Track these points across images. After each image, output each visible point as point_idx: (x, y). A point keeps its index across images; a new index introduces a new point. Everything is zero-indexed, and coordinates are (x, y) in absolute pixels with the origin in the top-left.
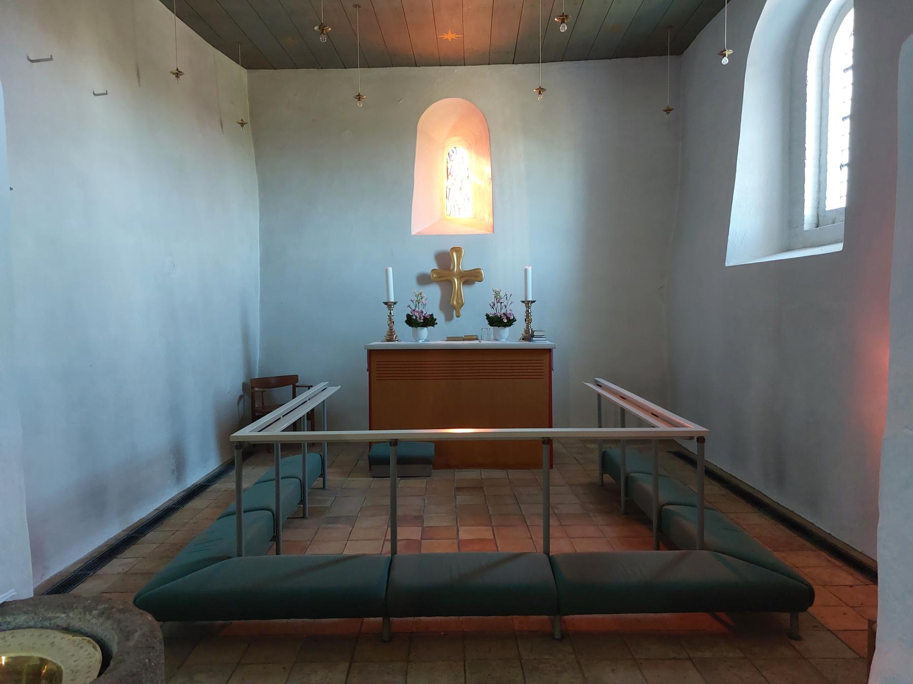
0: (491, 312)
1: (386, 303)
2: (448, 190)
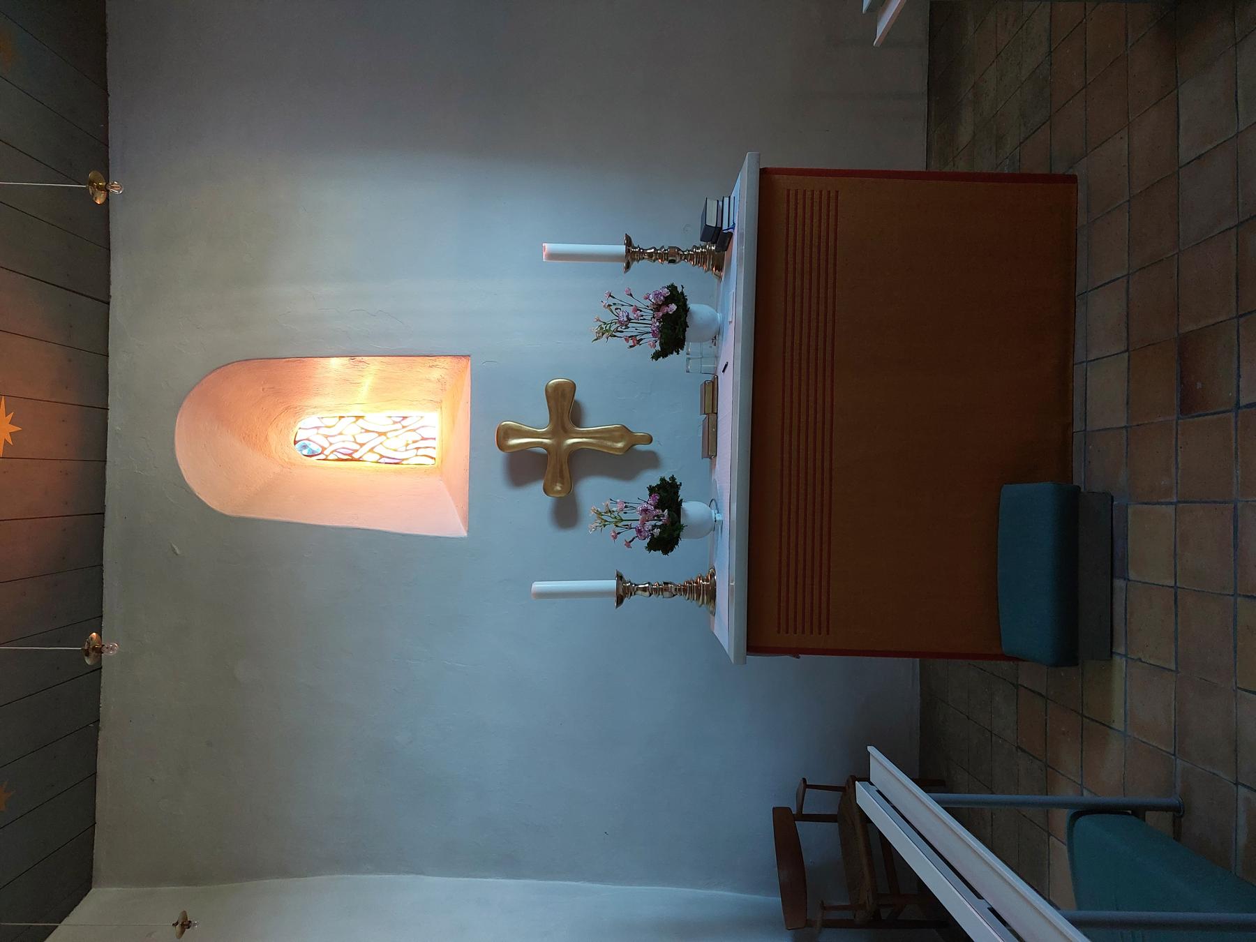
0: (650, 344)
1: (620, 600)
2: (382, 460)
